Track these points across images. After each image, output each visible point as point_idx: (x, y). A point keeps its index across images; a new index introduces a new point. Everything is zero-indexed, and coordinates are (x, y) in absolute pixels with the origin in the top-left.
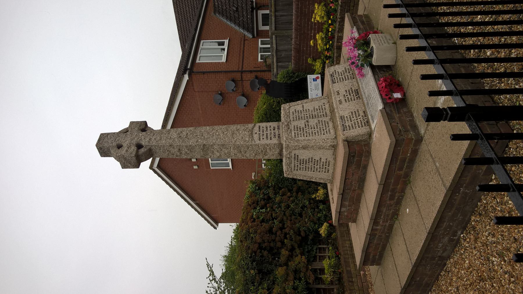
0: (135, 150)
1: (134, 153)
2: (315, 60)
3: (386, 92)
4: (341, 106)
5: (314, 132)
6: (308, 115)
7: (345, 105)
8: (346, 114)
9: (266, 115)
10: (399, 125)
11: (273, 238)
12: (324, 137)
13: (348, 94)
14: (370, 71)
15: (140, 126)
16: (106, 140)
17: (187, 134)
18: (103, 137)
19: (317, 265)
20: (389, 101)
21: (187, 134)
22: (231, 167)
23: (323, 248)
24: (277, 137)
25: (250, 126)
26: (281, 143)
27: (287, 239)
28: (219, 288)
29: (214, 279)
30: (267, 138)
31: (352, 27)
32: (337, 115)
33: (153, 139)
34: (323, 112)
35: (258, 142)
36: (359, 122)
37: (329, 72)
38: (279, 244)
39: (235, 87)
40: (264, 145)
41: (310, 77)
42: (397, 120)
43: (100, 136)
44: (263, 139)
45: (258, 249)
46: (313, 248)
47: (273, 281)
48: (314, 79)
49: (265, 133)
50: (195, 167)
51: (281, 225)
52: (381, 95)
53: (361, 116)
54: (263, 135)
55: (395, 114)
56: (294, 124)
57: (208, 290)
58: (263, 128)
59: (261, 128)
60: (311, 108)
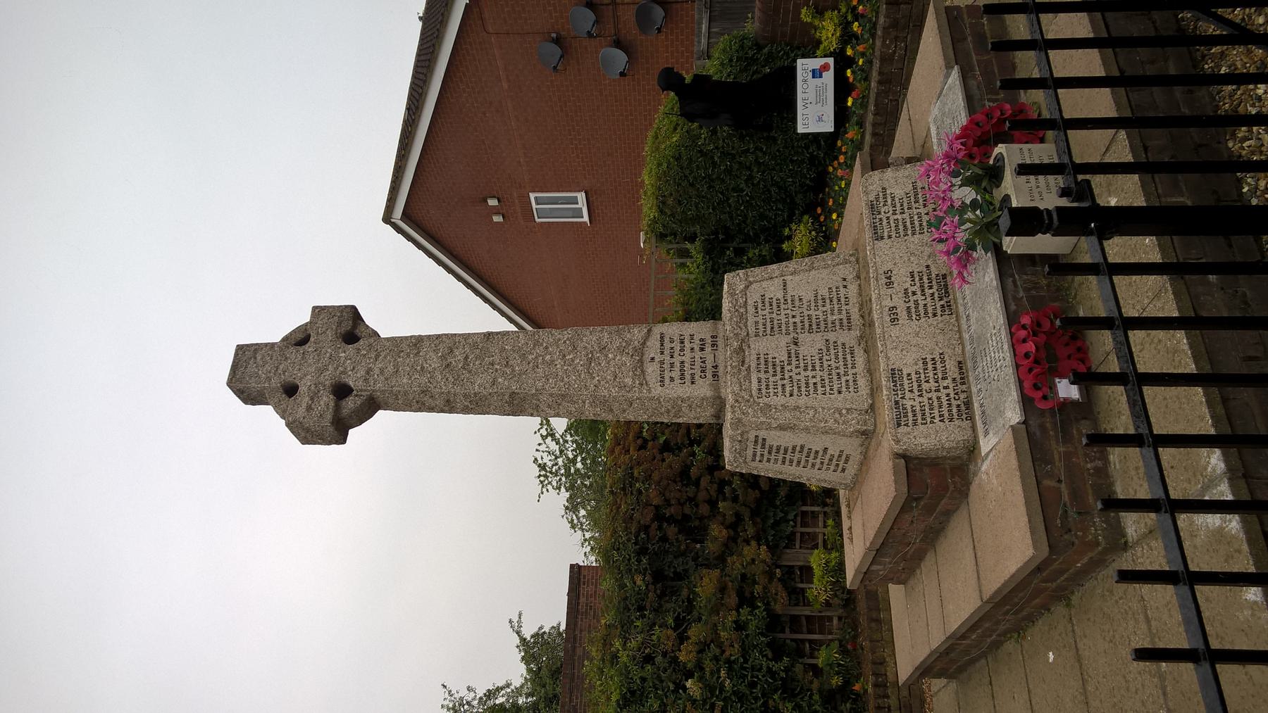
0: (332, 404)
1: (329, 416)
2: (819, 12)
3: (1037, 376)
4: (894, 332)
5: (811, 381)
6: (797, 320)
7: (907, 327)
8: (908, 363)
9: (678, 159)
10: (1063, 486)
11: (691, 495)
12: (839, 401)
13: (917, 288)
14: (991, 264)
15: (339, 324)
16: (252, 368)
17: (467, 358)
18: (246, 356)
19: (794, 557)
20: (1042, 405)
21: (467, 358)
22: (586, 218)
23: (813, 512)
24: (709, 375)
25: (637, 333)
26: (720, 397)
27: (725, 499)
28: (561, 452)
29: (553, 435)
30: (682, 377)
31: (949, 67)
32: (882, 366)
33: (377, 371)
34: (840, 311)
35: (657, 391)
36: (944, 399)
37: (866, 193)
38: (704, 509)
39: (597, 22)
40: (675, 400)
41: (804, 66)
42: (1060, 465)
43: (236, 354)
44: (672, 379)
45: (653, 521)
46: (786, 513)
47: (688, 599)
48: (813, 71)
49: (677, 360)
50: (497, 219)
51: (710, 459)
52: (1020, 382)
53: (949, 381)
54: (672, 365)
55: (1053, 442)
56: (759, 346)
57: (538, 455)
58: (672, 341)
59: (667, 340)
60: (808, 295)
